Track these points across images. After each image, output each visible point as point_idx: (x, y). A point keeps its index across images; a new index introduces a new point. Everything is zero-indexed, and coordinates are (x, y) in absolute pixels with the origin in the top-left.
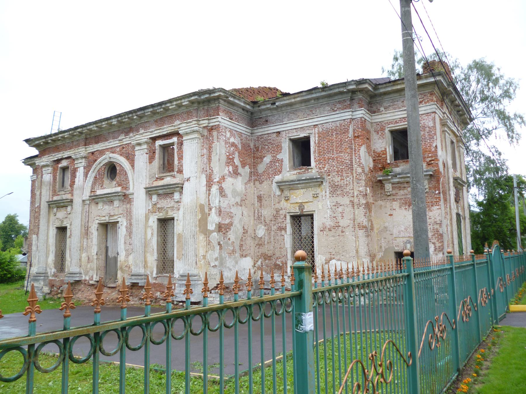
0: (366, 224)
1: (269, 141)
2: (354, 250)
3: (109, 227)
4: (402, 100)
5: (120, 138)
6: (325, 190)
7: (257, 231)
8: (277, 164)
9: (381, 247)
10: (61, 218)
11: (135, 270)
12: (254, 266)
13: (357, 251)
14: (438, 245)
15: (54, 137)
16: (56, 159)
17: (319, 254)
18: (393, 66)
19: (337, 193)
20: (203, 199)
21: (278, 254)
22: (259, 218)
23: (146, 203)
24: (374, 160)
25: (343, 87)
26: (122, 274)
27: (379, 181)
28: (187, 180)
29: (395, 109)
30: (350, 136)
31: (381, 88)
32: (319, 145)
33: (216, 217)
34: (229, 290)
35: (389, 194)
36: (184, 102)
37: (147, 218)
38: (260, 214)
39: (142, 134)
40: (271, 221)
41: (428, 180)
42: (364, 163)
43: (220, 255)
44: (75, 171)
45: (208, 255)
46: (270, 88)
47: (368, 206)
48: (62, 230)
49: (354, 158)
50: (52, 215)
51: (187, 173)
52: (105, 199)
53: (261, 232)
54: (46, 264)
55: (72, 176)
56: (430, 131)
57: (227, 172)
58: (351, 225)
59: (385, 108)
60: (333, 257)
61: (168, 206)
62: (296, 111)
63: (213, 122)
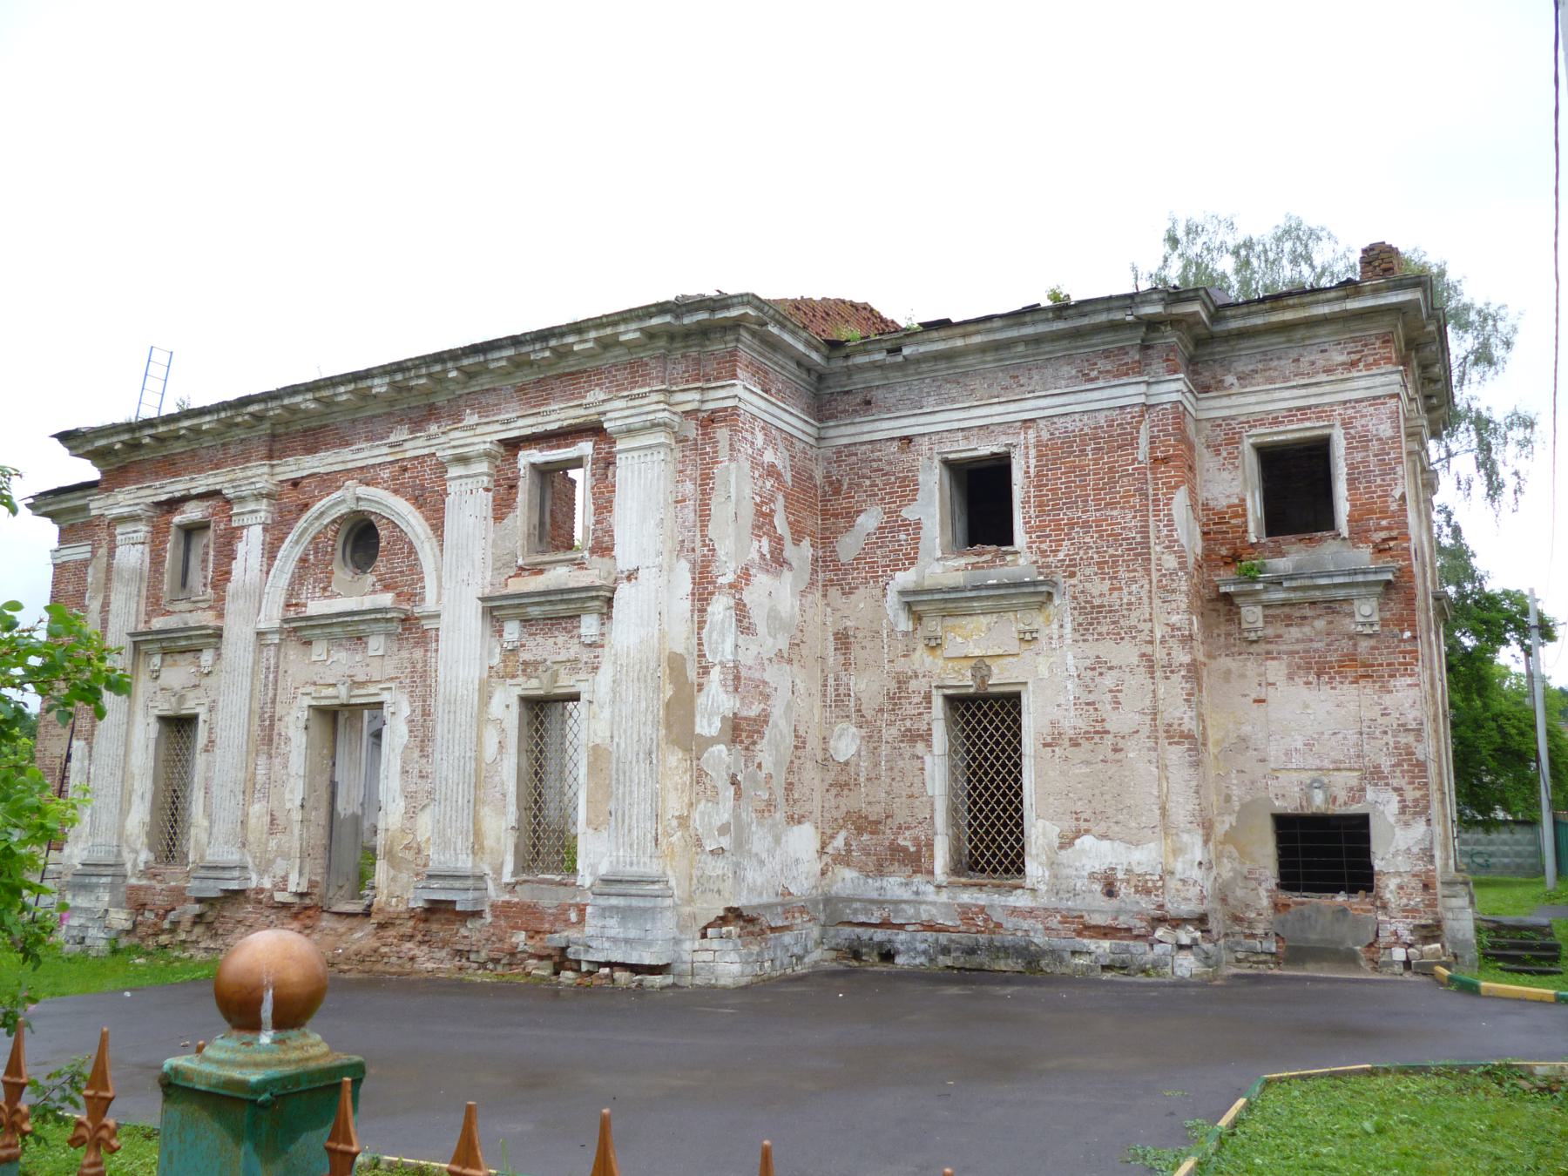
0: (1194, 728)
1: (875, 465)
2: (1155, 807)
3: (341, 720)
4: (1294, 354)
5: (393, 438)
9: (1228, 799)
10: (177, 687)
11: (438, 860)
12: (822, 851)
13: (1163, 809)
14: (1411, 794)
15: (161, 429)
16: (164, 497)
17: (1038, 817)
18: (1166, 260)
19: (1100, 629)
20: (680, 638)
21: (901, 817)
22: (839, 702)
23: (482, 647)
24: (1205, 533)
26: (392, 873)
27: (1222, 597)
28: (629, 578)
29: (1271, 380)
30: (1141, 458)
31: (1234, 317)
32: (1039, 480)
33: (723, 697)
34: (757, 929)
35: (1253, 636)
36: (626, 332)
37: (485, 696)
38: (842, 690)
39: (471, 428)
40: (882, 710)
41: (1379, 596)
42: (1184, 541)
43: (737, 817)
44: (230, 539)
45: (696, 815)
46: (853, 305)
47: (1194, 671)
48: (179, 726)
51: (625, 555)
52: (337, 630)
53: (847, 745)
54: (120, 836)
55: (218, 552)
56: (1383, 452)
57: (757, 557)
58: (1145, 730)
59: (1239, 378)
60: (1083, 825)
62: (966, 374)
63: (718, 399)
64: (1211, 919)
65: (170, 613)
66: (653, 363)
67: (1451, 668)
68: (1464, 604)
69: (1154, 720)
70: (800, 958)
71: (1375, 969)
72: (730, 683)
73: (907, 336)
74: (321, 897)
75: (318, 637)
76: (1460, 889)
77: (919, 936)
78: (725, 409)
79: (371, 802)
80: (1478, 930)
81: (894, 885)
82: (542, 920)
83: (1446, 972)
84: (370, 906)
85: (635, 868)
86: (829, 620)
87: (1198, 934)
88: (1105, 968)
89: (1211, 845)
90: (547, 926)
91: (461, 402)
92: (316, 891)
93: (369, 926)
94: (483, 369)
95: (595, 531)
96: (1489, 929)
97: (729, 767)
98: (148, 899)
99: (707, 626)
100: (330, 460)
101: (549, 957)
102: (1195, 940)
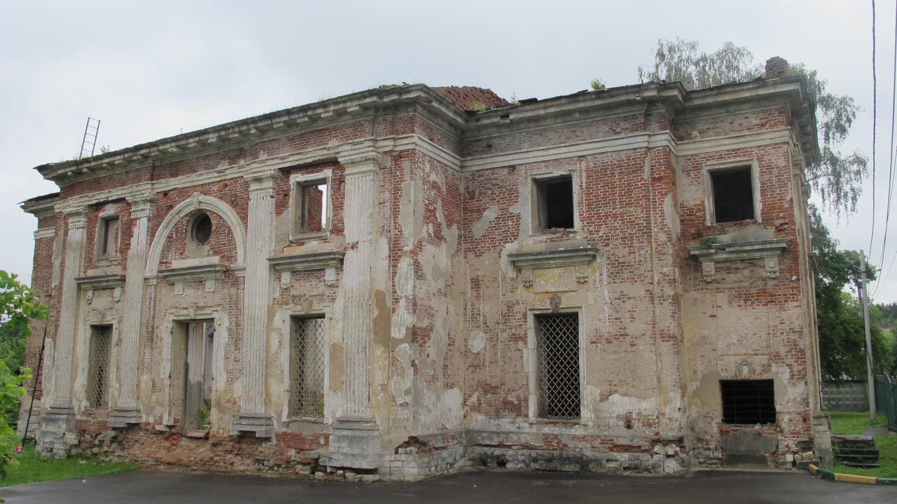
1: (494, 182)
4: (730, 119)
5: (219, 168)
6: (600, 270)
7: (470, 342)
8: (510, 223)
9: (695, 372)
11: (246, 408)
13: (659, 380)
14: (796, 368)
16: (94, 202)
17: (588, 384)
20: (382, 283)
21: (509, 384)
24: (682, 221)
25: (634, 93)
26: (220, 415)
29: (717, 134)
31: (697, 98)
34: (427, 449)
35: (709, 279)
36: (350, 107)
37: (271, 315)
39: (263, 162)
42: (670, 225)
43: (415, 384)
46: (481, 90)
47: (676, 300)
48: (102, 331)
49: (652, 216)
50: (83, 303)
51: (351, 233)
52: (188, 277)
53: (478, 343)
56: (780, 175)
58: (649, 334)
59: (700, 133)
60: (614, 388)
61: (313, 294)
62: (545, 130)
63: (403, 144)
64: (685, 440)
65: (97, 267)
66: (366, 124)
67: (818, 296)
68: (824, 260)
69: (654, 327)
70: (452, 465)
71: (776, 467)
72: (411, 308)
73: (512, 108)
74: (182, 428)
75: (178, 281)
76: (824, 421)
77: (520, 452)
78: (408, 150)
79: (207, 374)
80: (833, 443)
81: (506, 423)
82: (304, 443)
83: (816, 468)
84: (208, 433)
85: (357, 414)
86: (468, 271)
87: (678, 449)
88: (625, 469)
89: (685, 399)
90: (307, 446)
91: (258, 147)
92: (178, 424)
93: (208, 446)
94: (270, 128)
95: (333, 220)
96: (839, 443)
97: (410, 356)
98: (87, 428)
99: (398, 275)
100: (185, 181)
101: (309, 464)
102: (676, 452)
